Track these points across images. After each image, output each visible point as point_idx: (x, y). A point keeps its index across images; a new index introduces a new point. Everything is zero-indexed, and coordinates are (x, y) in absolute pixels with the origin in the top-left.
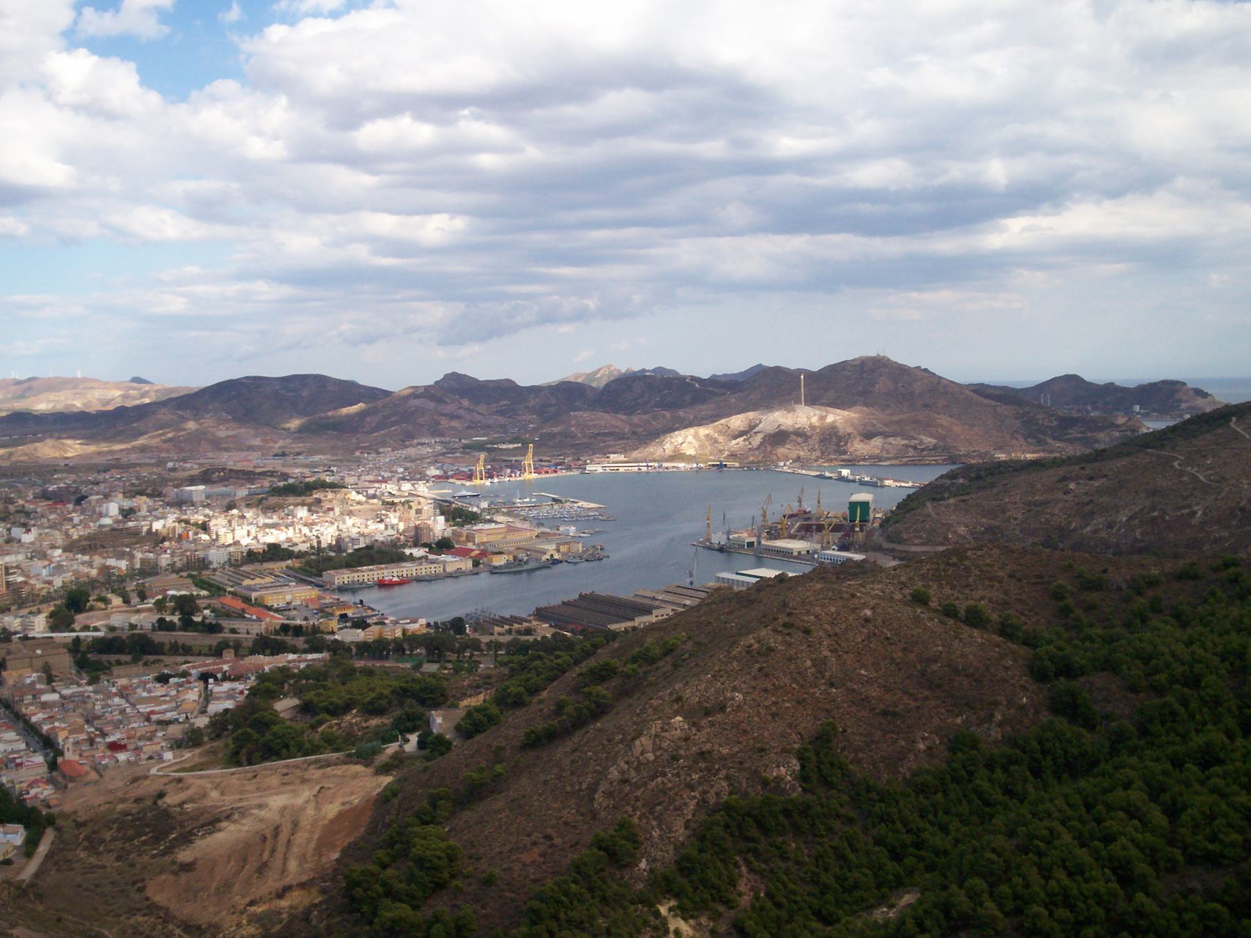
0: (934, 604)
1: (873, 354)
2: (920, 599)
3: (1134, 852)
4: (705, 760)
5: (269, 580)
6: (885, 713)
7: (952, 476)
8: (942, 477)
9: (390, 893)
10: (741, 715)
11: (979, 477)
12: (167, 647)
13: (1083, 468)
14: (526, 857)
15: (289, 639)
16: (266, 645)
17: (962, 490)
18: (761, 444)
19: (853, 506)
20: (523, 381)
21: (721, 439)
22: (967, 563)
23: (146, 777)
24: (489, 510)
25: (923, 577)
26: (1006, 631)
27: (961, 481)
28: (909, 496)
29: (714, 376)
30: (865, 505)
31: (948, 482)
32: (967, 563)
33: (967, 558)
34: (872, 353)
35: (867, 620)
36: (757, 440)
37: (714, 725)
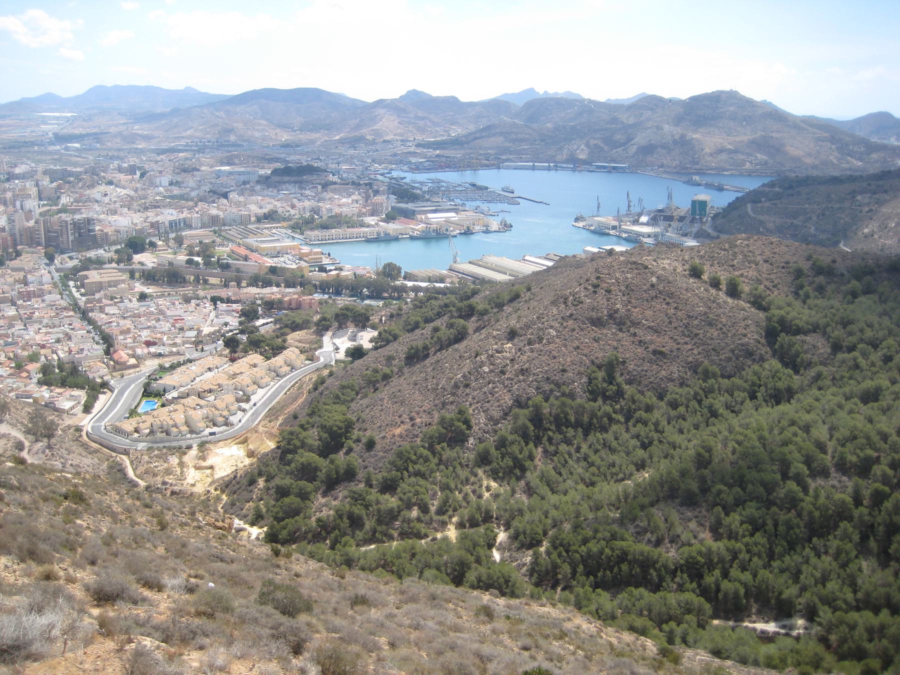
0: (705, 277)
1: (727, 89)
2: (696, 273)
3: (797, 455)
4: (523, 374)
5: (413, 160)
6: (655, 352)
7: (772, 185)
8: (764, 185)
9: (303, 445)
10: (552, 347)
11: (791, 187)
12: (751, 660)
13: (869, 185)
14: (398, 431)
15: (274, 278)
16: (256, 281)
17: (778, 196)
18: (636, 153)
19: (694, 203)
20: (464, 98)
21: (606, 148)
22: (736, 250)
23: (199, 170)
24: (429, 192)
25: (702, 257)
26: (758, 303)
27: (777, 189)
28: (737, 198)
29: (609, 100)
30: (703, 204)
31: (767, 189)
32: (736, 250)
33: (736, 246)
34: (727, 88)
35: (653, 286)
36: (633, 150)
37: (532, 352)
